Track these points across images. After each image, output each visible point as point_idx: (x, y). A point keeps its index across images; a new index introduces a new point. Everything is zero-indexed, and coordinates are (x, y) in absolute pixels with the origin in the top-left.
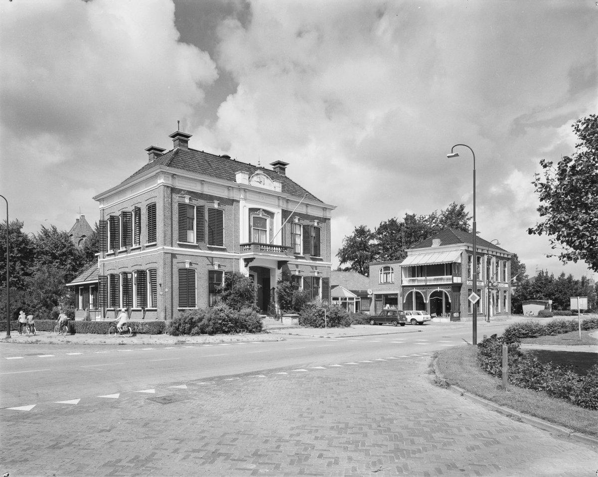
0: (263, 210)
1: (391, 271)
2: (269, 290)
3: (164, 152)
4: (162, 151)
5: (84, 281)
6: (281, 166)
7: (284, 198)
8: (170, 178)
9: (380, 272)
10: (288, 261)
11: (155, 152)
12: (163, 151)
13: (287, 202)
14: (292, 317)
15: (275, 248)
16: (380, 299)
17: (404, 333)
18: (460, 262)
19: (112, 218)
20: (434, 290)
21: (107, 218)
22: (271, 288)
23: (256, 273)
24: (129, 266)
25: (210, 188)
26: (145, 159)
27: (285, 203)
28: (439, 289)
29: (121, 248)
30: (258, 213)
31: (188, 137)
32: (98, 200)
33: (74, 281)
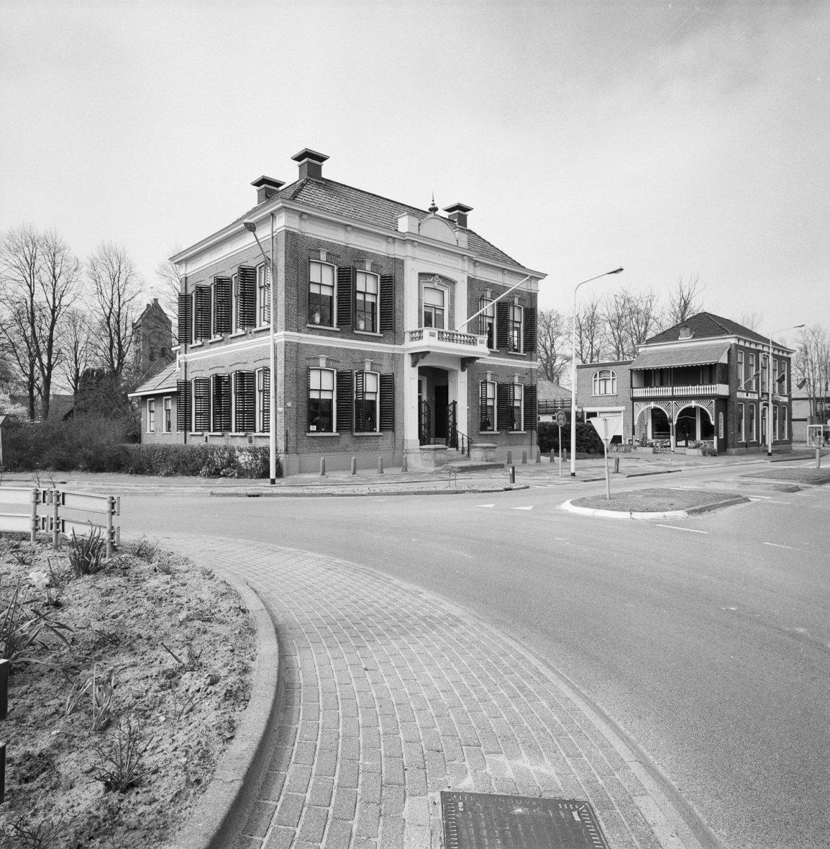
0: (441, 277)
1: (611, 378)
2: (447, 404)
3: (281, 188)
4: (278, 184)
5: (154, 390)
6: (459, 213)
7: (470, 259)
8: (297, 217)
9: (593, 379)
10: (478, 358)
11: (267, 187)
12: (281, 185)
13: (475, 266)
14: (435, 449)
15: (462, 337)
16: (266, 434)
17: (715, 481)
18: (726, 362)
19: (201, 290)
20: (687, 406)
21: (191, 289)
22: (450, 401)
23: (426, 378)
24: (227, 366)
25: (358, 238)
26: (251, 197)
27: (472, 266)
28: (693, 404)
29: (213, 336)
30: (432, 279)
31: (322, 159)
32: (177, 263)
33: (139, 390)
